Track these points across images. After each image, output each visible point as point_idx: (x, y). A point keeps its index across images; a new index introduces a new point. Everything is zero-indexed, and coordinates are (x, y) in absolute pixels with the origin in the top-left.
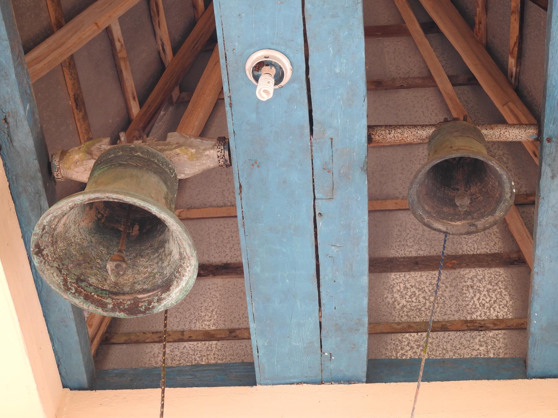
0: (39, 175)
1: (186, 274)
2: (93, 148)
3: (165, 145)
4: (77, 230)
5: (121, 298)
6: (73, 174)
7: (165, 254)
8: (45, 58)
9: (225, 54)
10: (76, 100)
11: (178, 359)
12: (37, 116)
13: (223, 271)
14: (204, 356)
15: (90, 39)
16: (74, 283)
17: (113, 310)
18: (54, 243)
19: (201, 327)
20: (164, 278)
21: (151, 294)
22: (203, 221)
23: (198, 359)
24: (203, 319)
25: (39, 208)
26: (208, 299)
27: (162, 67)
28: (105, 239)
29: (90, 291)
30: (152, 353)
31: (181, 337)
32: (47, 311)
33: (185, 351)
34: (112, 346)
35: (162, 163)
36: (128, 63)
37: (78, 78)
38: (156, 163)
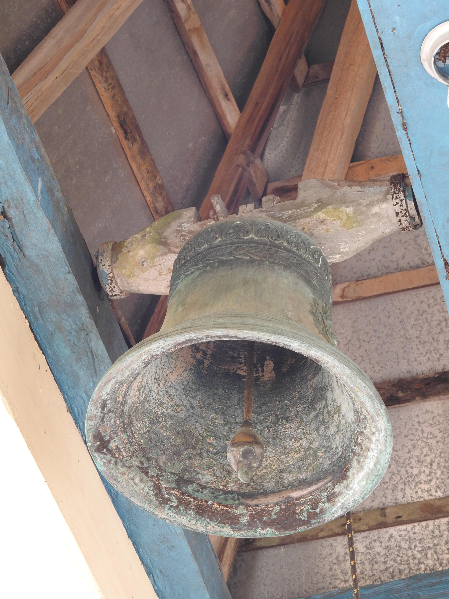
0: (80, 298)
1: (372, 446)
2: (169, 232)
3: (297, 208)
4: (164, 392)
5: (262, 501)
6: (140, 285)
7: (328, 412)
8: (55, 65)
9: (380, 39)
10: (122, 124)
11: (382, 559)
12: (59, 195)
13: (439, 387)
14: (429, 548)
15: (129, 14)
16: (173, 489)
17: (251, 525)
18: (126, 426)
19: (414, 495)
20: (333, 455)
21: (314, 487)
22: (388, 297)
23: (419, 556)
24: (417, 480)
25: (90, 354)
26: (420, 442)
27: (269, 29)
28: (216, 397)
29: (205, 498)
30: (334, 556)
31: (381, 519)
32: (133, 527)
33: (392, 543)
34: (260, 552)
35: (297, 246)
36: (205, 36)
37: (119, 84)
38: (285, 248)
